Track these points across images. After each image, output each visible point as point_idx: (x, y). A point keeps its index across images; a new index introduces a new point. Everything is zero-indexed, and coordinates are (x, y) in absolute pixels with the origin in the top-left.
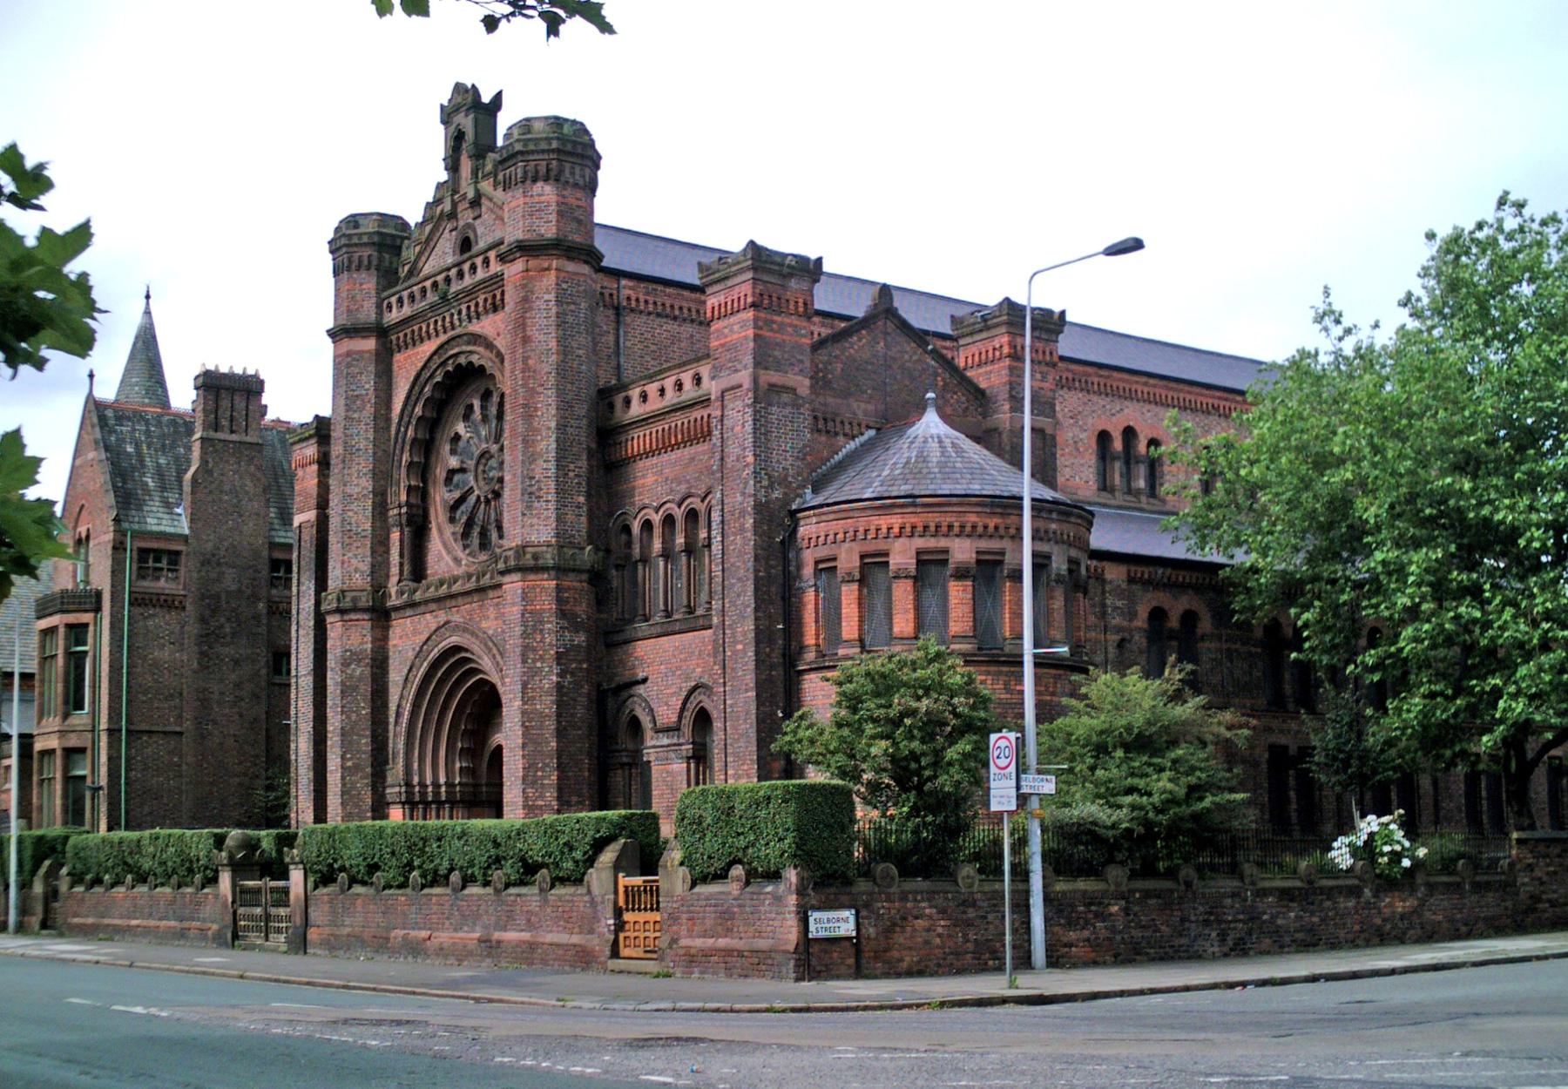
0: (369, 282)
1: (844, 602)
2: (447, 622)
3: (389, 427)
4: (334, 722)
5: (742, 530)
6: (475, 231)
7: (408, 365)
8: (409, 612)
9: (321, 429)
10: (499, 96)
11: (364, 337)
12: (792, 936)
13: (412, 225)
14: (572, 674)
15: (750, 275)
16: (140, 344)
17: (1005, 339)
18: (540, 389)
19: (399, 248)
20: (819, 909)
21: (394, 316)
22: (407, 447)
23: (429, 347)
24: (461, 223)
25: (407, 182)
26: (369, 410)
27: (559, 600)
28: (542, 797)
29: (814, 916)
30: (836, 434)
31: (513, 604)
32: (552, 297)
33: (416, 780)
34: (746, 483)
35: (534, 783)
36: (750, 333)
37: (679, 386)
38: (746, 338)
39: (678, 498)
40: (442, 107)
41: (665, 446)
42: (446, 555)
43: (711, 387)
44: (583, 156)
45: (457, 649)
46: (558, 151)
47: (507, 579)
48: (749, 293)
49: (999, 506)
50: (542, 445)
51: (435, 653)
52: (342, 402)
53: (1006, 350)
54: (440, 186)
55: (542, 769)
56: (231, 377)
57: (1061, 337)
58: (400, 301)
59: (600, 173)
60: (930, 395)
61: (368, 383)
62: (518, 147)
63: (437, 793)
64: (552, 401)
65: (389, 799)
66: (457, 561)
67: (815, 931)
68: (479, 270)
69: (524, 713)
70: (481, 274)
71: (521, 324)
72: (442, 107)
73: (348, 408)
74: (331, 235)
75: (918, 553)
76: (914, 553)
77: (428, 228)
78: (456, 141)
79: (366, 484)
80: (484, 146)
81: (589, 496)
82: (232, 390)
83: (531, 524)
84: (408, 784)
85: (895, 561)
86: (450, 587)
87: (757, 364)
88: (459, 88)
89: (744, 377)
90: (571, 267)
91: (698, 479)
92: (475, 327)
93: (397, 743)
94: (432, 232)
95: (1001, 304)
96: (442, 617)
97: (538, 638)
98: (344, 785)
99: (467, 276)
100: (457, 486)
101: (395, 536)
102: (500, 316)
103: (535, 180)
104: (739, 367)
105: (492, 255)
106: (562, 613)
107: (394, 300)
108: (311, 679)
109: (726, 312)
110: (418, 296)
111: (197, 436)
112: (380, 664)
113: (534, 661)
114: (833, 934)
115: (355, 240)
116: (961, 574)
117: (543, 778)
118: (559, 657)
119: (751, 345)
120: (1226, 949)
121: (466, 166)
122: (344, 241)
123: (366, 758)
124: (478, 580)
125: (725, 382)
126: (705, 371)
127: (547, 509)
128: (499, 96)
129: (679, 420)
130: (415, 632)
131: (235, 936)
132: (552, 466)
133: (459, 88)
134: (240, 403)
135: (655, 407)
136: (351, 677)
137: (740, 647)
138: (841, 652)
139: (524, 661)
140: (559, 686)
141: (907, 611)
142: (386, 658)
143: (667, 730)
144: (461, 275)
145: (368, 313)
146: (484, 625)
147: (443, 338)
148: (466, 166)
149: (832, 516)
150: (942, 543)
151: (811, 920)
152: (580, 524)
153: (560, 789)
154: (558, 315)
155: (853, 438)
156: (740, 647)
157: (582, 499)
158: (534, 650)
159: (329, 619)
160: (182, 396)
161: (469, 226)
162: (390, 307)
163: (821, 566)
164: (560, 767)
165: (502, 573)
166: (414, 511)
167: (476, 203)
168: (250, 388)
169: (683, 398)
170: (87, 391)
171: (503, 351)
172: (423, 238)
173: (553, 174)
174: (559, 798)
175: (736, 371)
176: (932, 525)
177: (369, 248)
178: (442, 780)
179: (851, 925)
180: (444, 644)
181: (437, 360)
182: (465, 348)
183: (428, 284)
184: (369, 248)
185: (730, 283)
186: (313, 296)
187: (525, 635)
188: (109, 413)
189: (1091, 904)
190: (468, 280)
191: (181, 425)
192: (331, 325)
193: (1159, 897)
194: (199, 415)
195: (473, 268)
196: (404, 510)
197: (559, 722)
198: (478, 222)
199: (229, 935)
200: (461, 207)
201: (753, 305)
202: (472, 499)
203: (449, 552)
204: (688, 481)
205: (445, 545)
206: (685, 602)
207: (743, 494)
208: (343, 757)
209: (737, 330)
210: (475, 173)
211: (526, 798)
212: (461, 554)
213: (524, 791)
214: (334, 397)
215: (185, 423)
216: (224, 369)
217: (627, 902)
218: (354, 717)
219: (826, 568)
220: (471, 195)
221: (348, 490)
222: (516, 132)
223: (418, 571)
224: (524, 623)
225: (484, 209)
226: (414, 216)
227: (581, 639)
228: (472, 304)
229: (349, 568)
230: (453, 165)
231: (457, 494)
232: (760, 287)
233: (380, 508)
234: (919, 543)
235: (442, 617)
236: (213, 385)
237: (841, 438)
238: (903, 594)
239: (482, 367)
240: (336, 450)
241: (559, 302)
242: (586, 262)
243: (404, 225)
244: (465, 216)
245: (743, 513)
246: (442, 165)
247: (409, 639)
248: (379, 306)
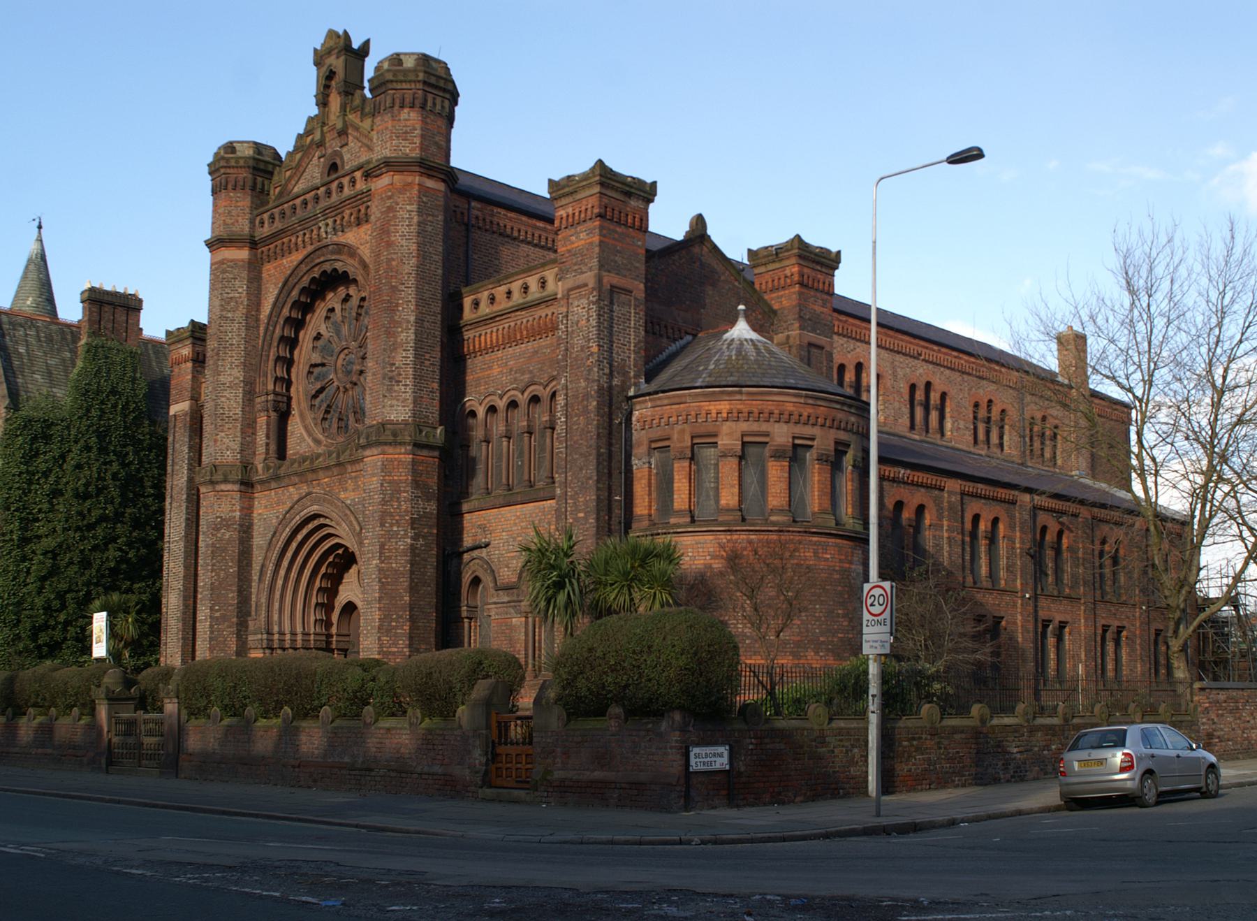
0: (244, 202)
1: (676, 477)
2: (309, 494)
3: (258, 327)
4: (204, 579)
6: (342, 158)
7: (274, 274)
9: (197, 332)
10: (367, 43)
12: (676, 768)
14: (424, 537)
15: (597, 189)
16: (32, 267)
17: (796, 269)
18: (402, 287)
19: (272, 174)
20: (697, 745)
21: (267, 230)
23: (296, 257)
24: (329, 151)
25: (280, 114)
27: (414, 472)
28: (395, 644)
29: (695, 751)
30: (661, 336)
32: (414, 207)
33: (276, 629)
34: (590, 371)
35: (388, 631)
36: (596, 239)
37: (526, 288)
39: (521, 386)
40: (315, 50)
41: (511, 339)
42: (302, 436)
44: (445, 90)
45: (316, 516)
47: (368, 452)
48: (597, 203)
49: (812, 397)
52: (217, 303)
53: (796, 278)
54: (310, 120)
55: (396, 620)
56: (115, 294)
57: (837, 272)
58: (272, 218)
59: (456, 108)
60: (741, 307)
63: (294, 641)
69: (381, 570)
70: (347, 191)
71: (384, 232)
72: (315, 50)
73: (223, 308)
74: (210, 159)
75: (742, 436)
77: (298, 156)
78: (327, 80)
79: (237, 374)
80: (352, 86)
81: (441, 384)
83: (395, 402)
84: (269, 633)
86: (312, 462)
87: (601, 266)
88: (332, 34)
89: (589, 277)
90: (430, 183)
91: (541, 369)
92: (341, 238)
93: (258, 595)
94: (301, 159)
95: (793, 240)
98: (212, 632)
99: (334, 194)
100: (317, 379)
101: (262, 420)
102: (366, 228)
103: (402, 107)
104: (584, 269)
105: (358, 174)
106: (416, 484)
107: (266, 216)
108: (182, 544)
109: (573, 223)
110: (288, 213)
111: (83, 342)
112: (246, 529)
113: (392, 525)
115: (233, 163)
116: (778, 455)
119: (597, 250)
120: (1008, 776)
121: (335, 101)
122: (223, 163)
123: (232, 610)
124: (338, 456)
125: (570, 283)
126: (550, 275)
127: (406, 390)
128: (367, 43)
129: (525, 318)
130: (280, 502)
131: (110, 763)
133: (332, 34)
134: (121, 316)
135: (501, 307)
136: (221, 540)
137: (581, 515)
138: (672, 521)
139: (382, 525)
141: (733, 486)
142: (250, 526)
143: (509, 588)
144: (329, 193)
146: (342, 495)
147: (310, 248)
148: (335, 101)
150: (764, 427)
151: (692, 755)
152: (433, 410)
153: (411, 638)
155: (675, 340)
156: (581, 515)
157: (436, 386)
158: (391, 515)
159: (203, 490)
160: (70, 310)
161: (336, 153)
162: (262, 223)
163: (654, 445)
164: (412, 619)
165: (364, 447)
166: (279, 398)
167: (343, 133)
168: (129, 306)
169: (529, 298)
171: (367, 261)
172: (294, 165)
173: (417, 103)
174: (410, 646)
175: (583, 273)
177: (246, 174)
178: (299, 629)
179: (725, 760)
180: (305, 513)
181: (304, 268)
182: (329, 257)
185: (578, 197)
186: (195, 210)
187: (384, 502)
191: (70, 331)
192: (208, 236)
193: (962, 732)
196: (271, 397)
197: (412, 580)
198: (345, 149)
199: (103, 761)
200: (328, 137)
201: (600, 215)
202: (330, 390)
203: (310, 434)
204: (531, 372)
205: (306, 428)
206: (526, 477)
207: (587, 379)
208: (212, 609)
211: (381, 646)
212: (321, 437)
213: (379, 639)
214: (210, 299)
216: (108, 288)
217: (500, 737)
218: (222, 574)
220: (339, 125)
221: (222, 378)
222: (386, 66)
223: (282, 453)
224: (383, 492)
225: (350, 138)
226: (284, 146)
227: (432, 507)
228: (338, 218)
229: (222, 446)
230: (322, 101)
232: (605, 201)
234: (744, 426)
236: (96, 300)
237: (665, 340)
238: (729, 469)
239: (345, 272)
240: (211, 344)
241: (420, 213)
242: (444, 181)
243: (277, 155)
244: (333, 145)
246: (314, 100)
247: (270, 510)
248: (252, 222)
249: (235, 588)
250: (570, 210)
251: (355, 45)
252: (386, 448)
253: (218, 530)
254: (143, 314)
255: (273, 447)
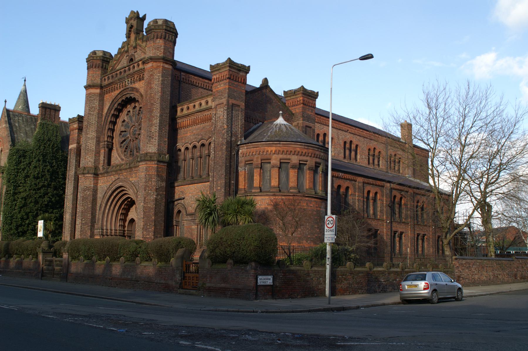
5: (222, 150)
7: (108, 99)
8: (106, 175)
9: (80, 119)
11: (96, 88)
12: (252, 284)
13: (113, 55)
14: (160, 195)
15: (228, 68)
17: (301, 98)
20: (261, 275)
22: (108, 124)
23: (117, 92)
24: (130, 54)
25: (113, 41)
26: (96, 111)
28: (149, 235)
31: (142, 172)
32: (160, 75)
33: (105, 228)
35: (146, 230)
36: (227, 87)
38: (225, 88)
41: (195, 123)
42: (116, 157)
43: (211, 104)
46: (166, 30)
47: (141, 164)
48: (228, 74)
49: (307, 146)
50: (155, 121)
51: (114, 188)
53: (302, 102)
54: (124, 43)
55: (149, 226)
56: (51, 105)
57: (317, 100)
58: (109, 78)
61: (96, 103)
62: (153, 27)
64: (159, 107)
65: (95, 233)
66: (122, 159)
67: (260, 282)
68: (136, 68)
69: (144, 207)
71: (149, 83)
74: (87, 57)
76: (279, 159)
77: (119, 56)
78: (130, 29)
80: (139, 31)
81: (168, 139)
82: (50, 109)
83: (151, 145)
85: (273, 162)
87: (229, 97)
88: (132, 12)
89: (224, 101)
92: (133, 86)
93: (99, 215)
94: (120, 57)
96: (117, 177)
97: (150, 183)
98: (81, 229)
100: (123, 136)
101: (102, 151)
102: (142, 82)
103: (157, 38)
105: (140, 63)
106: (158, 175)
109: (219, 81)
110: (114, 76)
111: (39, 122)
112: (95, 191)
113: (149, 190)
114: (265, 284)
115: (95, 58)
116: (293, 167)
117: (149, 228)
118: (156, 189)
119: (227, 90)
121: (133, 36)
122: (91, 58)
124: (130, 165)
127: (155, 141)
129: (200, 115)
132: (157, 128)
133: (132, 12)
134: (53, 113)
136: (86, 194)
139: (145, 190)
140: (156, 199)
143: (191, 215)
144: (129, 69)
145: (98, 81)
147: (122, 89)
148: (133, 36)
149: (252, 147)
151: (259, 279)
152: (165, 149)
153: (154, 232)
154: (162, 80)
155: (255, 124)
156: (219, 188)
157: (166, 140)
158: (148, 187)
159: (80, 176)
160: (35, 110)
162: (105, 80)
163: (247, 163)
164: (155, 225)
165: (139, 162)
167: (135, 48)
168: (56, 109)
169: (202, 108)
170: (4, 106)
173: (163, 37)
174: (154, 235)
176: (285, 150)
177: (100, 62)
179: (271, 281)
181: (119, 96)
182: (129, 92)
183: (118, 72)
184: (100, 62)
185: (221, 71)
186: (81, 75)
187: (146, 182)
188: (11, 113)
189: (343, 275)
190: (131, 71)
191: (34, 118)
192: (85, 84)
194: (40, 116)
195: (134, 67)
196: (106, 143)
197: (155, 211)
198: (136, 53)
202: (128, 141)
203: (120, 157)
204: (202, 135)
206: (199, 174)
208: (82, 220)
209: (222, 87)
210: (136, 39)
211: (143, 235)
214: (85, 107)
215: (35, 119)
216: (48, 102)
218: (86, 207)
219: (249, 163)
220: (134, 45)
221: (88, 136)
222: (152, 23)
223: (109, 163)
226: (114, 52)
227: (164, 184)
228: (133, 78)
229: (88, 160)
230: (128, 36)
231: (123, 139)
232: (231, 73)
233: (98, 142)
234: (281, 156)
235: (117, 177)
236: (44, 107)
238: (275, 172)
241: (162, 76)
242: (171, 65)
244: (131, 52)
245: (222, 144)
248: (101, 79)
249: (90, 213)
250: (218, 76)
251: (141, 16)
252: (147, 162)
253: (85, 191)
254: (61, 112)
255: (106, 161)
